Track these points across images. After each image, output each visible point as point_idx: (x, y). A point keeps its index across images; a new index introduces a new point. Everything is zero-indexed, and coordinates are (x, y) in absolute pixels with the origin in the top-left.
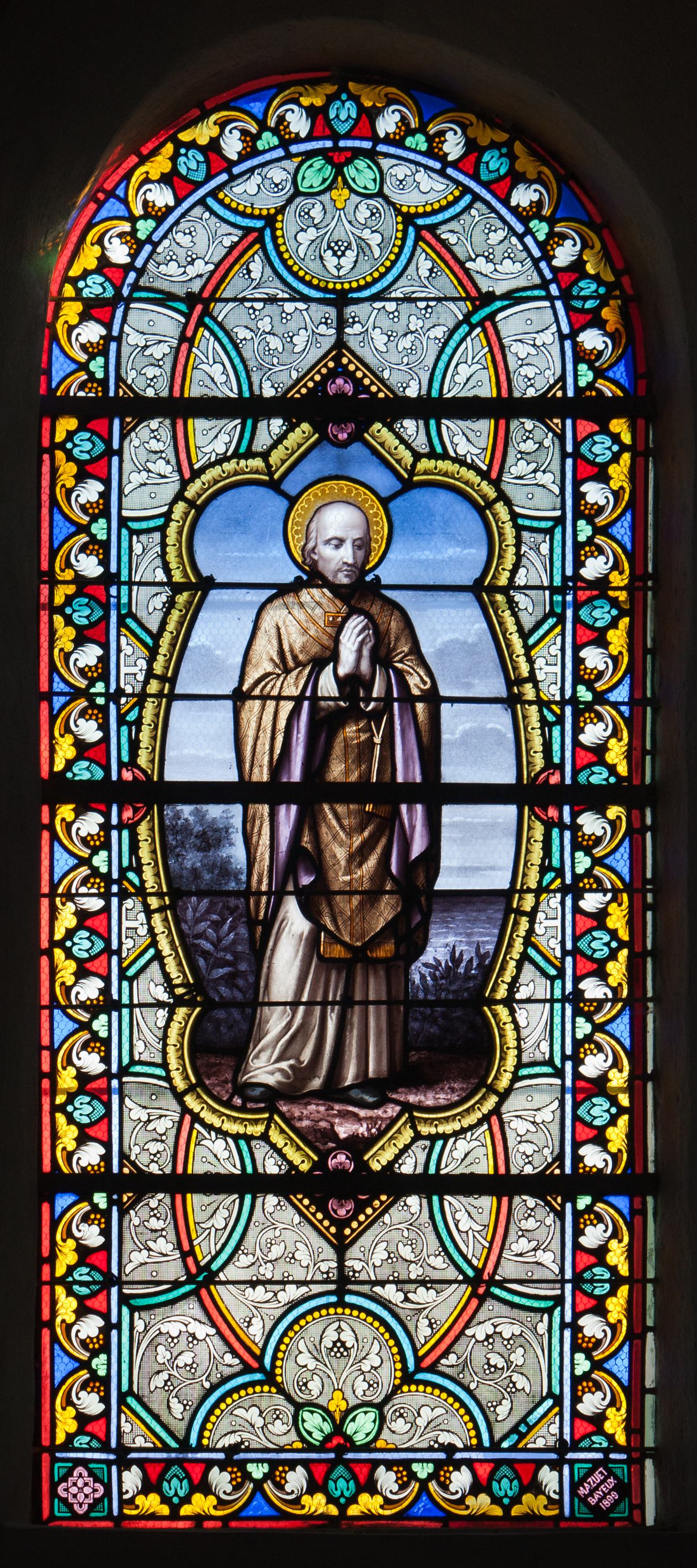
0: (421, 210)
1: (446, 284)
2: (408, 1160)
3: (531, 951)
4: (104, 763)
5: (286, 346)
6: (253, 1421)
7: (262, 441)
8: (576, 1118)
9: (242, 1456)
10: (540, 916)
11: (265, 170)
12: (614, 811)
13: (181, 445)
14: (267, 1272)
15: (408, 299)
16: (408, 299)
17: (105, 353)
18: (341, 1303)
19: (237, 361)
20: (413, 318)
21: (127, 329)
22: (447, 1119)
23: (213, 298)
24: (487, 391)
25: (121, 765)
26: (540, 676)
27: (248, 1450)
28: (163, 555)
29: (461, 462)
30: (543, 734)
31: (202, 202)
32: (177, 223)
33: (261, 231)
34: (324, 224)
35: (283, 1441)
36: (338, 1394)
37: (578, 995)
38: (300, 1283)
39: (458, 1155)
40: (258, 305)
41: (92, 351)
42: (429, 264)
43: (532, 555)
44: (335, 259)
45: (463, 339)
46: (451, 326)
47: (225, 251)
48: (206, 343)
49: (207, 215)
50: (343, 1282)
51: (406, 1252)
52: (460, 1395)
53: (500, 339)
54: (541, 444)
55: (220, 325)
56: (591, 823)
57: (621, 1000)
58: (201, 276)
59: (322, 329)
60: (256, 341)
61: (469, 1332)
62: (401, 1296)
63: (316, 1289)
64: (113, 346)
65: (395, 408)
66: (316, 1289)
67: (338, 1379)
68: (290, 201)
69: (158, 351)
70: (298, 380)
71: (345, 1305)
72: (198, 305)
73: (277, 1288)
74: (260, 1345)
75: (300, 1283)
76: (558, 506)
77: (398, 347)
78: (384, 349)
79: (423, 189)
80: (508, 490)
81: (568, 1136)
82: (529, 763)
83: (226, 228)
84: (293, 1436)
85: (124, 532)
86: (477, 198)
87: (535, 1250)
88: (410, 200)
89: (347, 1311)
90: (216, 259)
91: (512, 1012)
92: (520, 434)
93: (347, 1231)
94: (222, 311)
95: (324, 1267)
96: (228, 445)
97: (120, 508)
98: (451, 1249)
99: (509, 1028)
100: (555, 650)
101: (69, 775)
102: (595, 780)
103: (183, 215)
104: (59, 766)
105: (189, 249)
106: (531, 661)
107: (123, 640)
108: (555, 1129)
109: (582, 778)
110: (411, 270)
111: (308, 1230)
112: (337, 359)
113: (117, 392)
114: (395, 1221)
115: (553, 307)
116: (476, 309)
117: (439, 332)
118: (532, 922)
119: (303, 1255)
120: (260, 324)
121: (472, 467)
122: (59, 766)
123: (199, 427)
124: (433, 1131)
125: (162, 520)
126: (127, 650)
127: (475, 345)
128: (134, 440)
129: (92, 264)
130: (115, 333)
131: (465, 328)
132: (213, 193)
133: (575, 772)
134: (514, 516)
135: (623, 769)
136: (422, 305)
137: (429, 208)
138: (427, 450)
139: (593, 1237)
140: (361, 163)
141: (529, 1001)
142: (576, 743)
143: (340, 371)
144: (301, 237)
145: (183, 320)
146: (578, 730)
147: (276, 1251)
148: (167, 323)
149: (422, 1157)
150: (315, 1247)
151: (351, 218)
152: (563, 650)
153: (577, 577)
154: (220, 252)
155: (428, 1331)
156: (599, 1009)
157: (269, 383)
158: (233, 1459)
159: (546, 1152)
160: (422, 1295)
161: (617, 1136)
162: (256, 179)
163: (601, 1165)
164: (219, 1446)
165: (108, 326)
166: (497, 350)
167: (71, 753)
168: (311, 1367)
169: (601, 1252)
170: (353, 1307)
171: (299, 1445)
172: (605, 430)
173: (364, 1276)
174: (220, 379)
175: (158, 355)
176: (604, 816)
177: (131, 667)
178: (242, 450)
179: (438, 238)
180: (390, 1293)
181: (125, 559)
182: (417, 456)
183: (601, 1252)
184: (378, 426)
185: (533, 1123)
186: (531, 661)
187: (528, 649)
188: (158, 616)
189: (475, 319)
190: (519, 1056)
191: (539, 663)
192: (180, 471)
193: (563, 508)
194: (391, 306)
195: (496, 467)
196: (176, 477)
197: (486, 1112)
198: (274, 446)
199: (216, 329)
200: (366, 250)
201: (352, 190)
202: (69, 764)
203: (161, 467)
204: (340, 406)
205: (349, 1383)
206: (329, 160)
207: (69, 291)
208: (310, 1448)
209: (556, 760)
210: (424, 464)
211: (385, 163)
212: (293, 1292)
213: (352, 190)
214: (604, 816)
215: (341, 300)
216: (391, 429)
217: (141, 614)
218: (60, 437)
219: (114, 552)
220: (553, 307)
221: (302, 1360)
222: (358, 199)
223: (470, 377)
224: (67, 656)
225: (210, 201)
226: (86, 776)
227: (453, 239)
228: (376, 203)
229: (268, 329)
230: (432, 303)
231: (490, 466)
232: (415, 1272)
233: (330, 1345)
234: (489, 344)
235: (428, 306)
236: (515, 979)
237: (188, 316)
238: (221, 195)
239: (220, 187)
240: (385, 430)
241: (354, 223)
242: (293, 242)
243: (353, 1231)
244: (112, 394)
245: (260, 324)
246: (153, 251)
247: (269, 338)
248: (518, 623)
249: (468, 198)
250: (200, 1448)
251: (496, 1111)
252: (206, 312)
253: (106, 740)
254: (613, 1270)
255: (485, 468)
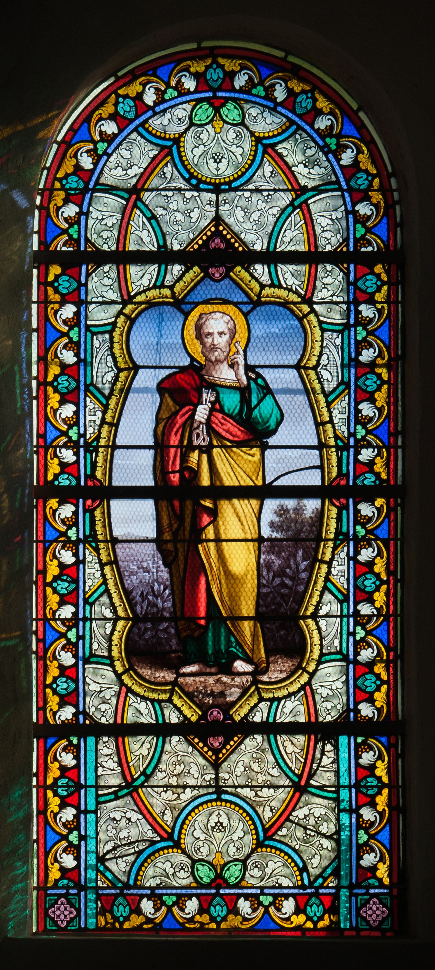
0: (266, 135)
1: (281, 182)
2: (257, 714)
3: (329, 585)
4: (76, 475)
5: (186, 219)
6: (167, 868)
7: (264, 707)
8: (356, 686)
9: (160, 891)
10: (335, 563)
11: (173, 110)
12: (380, 502)
13: (122, 280)
14: (173, 781)
15: (258, 190)
16: (258, 190)
17: (78, 223)
18: (219, 799)
19: (278, 756)
20: (260, 202)
21: (91, 209)
22: (280, 688)
23: (143, 189)
24: (302, 247)
25: (347, 508)
26: (97, 566)
27: (165, 888)
28: (321, 638)
29: (143, 698)
30: (337, 455)
31: (136, 129)
32: (120, 144)
33: (170, 147)
34: (209, 142)
35: (185, 883)
36: (218, 130)
37: (357, 613)
38: (193, 787)
39: (147, 276)
40: (170, 194)
41: (71, 222)
42: (165, 818)
43: (103, 642)
44: (221, 821)
45: (290, 215)
46: (282, 208)
47: (149, 160)
48: (139, 219)
49: (139, 138)
50: (219, 789)
51: (179, 217)
52: (288, 852)
53: (311, 215)
54: (97, 708)
55: (147, 206)
56: (366, 509)
57: (382, 615)
58: (300, 808)
59: (208, 208)
60: (266, 768)
61: (142, 170)
62: (253, 793)
63: (205, 791)
64: (83, 218)
65: (250, 258)
66: (205, 791)
67: (218, 139)
68: (187, 129)
69: (110, 222)
70: (193, 240)
71: (222, 800)
72: (134, 194)
73: (179, 790)
74: (171, 827)
75: (193, 787)
76: (345, 317)
77: (251, 220)
78: (192, 765)
79: (267, 123)
80: (116, 682)
81: (351, 699)
82: (329, 473)
83: (286, 839)
84: (191, 879)
85: (89, 334)
86: (299, 127)
87: (103, 219)
88: (259, 128)
89: (224, 804)
90: (144, 166)
91: (317, 624)
92: (109, 714)
93: (213, 229)
94: (148, 198)
95: (208, 777)
96: (284, 706)
97: (86, 319)
98: (282, 765)
99: (315, 633)
100: (89, 583)
101: (56, 483)
102: (366, 482)
103: (124, 139)
104: (50, 477)
105: (129, 159)
106: (103, 575)
107: (88, 399)
108: (344, 692)
109: (359, 482)
110: (260, 172)
111: (236, 229)
112: (218, 758)
113: (86, 248)
114: (248, 748)
115: (343, 195)
116: (298, 196)
117: (275, 211)
118: (330, 567)
119: (194, 770)
120: (264, 778)
121: (137, 695)
122: (50, 477)
123: (134, 270)
124: (271, 696)
125: (323, 660)
126: (90, 406)
127: (296, 218)
128: (94, 278)
129: (70, 170)
130: (85, 210)
131: (290, 209)
132: (142, 124)
133: (355, 478)
134: (321, 323)
135: (384, 476)
136: (265, 193)
137: (271, 134)
138: (269, 283)
139: (367, 758)
140: (206, 880)
141: (326, 616)
142: (356, 461)
143: (217, 234)
144: (195, 151)
145: (124, 203)
146: (357, 453)
147: (179, 769)
148: (116, 204)
149: (265, 710)
150: (232, 220)
151: (225, 138)
152: (84, 582)
153: (356, 360)
154: (147, 161)
155: (270, 814)
156: (369, 621)
157: (258, 741)
158: (154, 895)
159: (96, 279)
160: (266, 792)
161: (380, 697)
162: (168, 115)
163: (371, 715)
164: (147, 885)
165: (80, 206)
166: (123, 762)
167: (57, 470)
168: (235, 146)
169: (372, 768)
170: (227, 801)
171: (194, 885)
172: (373, 273)
173: (230, 783)
174: (147, 239)
175: (110, 224)
176: (373, 504)
177: (93, 416)
178: (158, 284)
179: (276, 151)
180: (247, 793)
181: (89, 351)
182: (263, 287)
183: (372, 768)
184: (239, 268)
185: (331, 689)
186: (103, 575)
187: (105, 582)
188: (109, 385)
189: (296, 203)
190: (321, 650)
191: (98, 575)
192: (312, 690)
193: (84, 669)
194: (247, 194)
195: (123, 694)
196: (314, 687)
197: (303, 683)
198: (178, 281)
199: (291, 774)
200: (234, 157)
201: (225, 122)
202: (56, 476)
203: (324, 692)
204: (218, 254)
205: (211, 138)
206: (211, 105)
207: (57, 185)
208: (234, 100)
209: (87, 515)
210: (165, 696)
211: (246, 106)
212: (189, 794)
213: (225, 122)
214: (373, 504)
215: (217, 189)
216: (185, 717)
217: (335, 602)
218: (51, 278)
219: (83, 347)
220: (343, 195)
221: (240, 150)
222: (229, 126)
223: (293, 239)
224: (55, 411)
225: (141, 129)
226: (67, 483)
227: (285, 153)
228: (197, 857)
229: (259, 775)
230: (271, 193)
231: (126, 696)
232: (261, 779)
233: (213, 825)
234: (129, 767)
235: (269, 195)
236: (319, 602)
237: (127, 200)
238: (147, 126)
239: (146, 121)
240: (189, 716)
241: (227, 142)
242: (190, 153)
243: (224, 755)
244: (82, 249)
245: (171, 206)
246: (107, 160)
247: (176, 214)
248: (110, 598)
249: (294, 127)
250: (136, 886)
251: (309, 683)
252: (139, 199)
253: (77, 462)
254: (379, 779)
255: (129, 695)
